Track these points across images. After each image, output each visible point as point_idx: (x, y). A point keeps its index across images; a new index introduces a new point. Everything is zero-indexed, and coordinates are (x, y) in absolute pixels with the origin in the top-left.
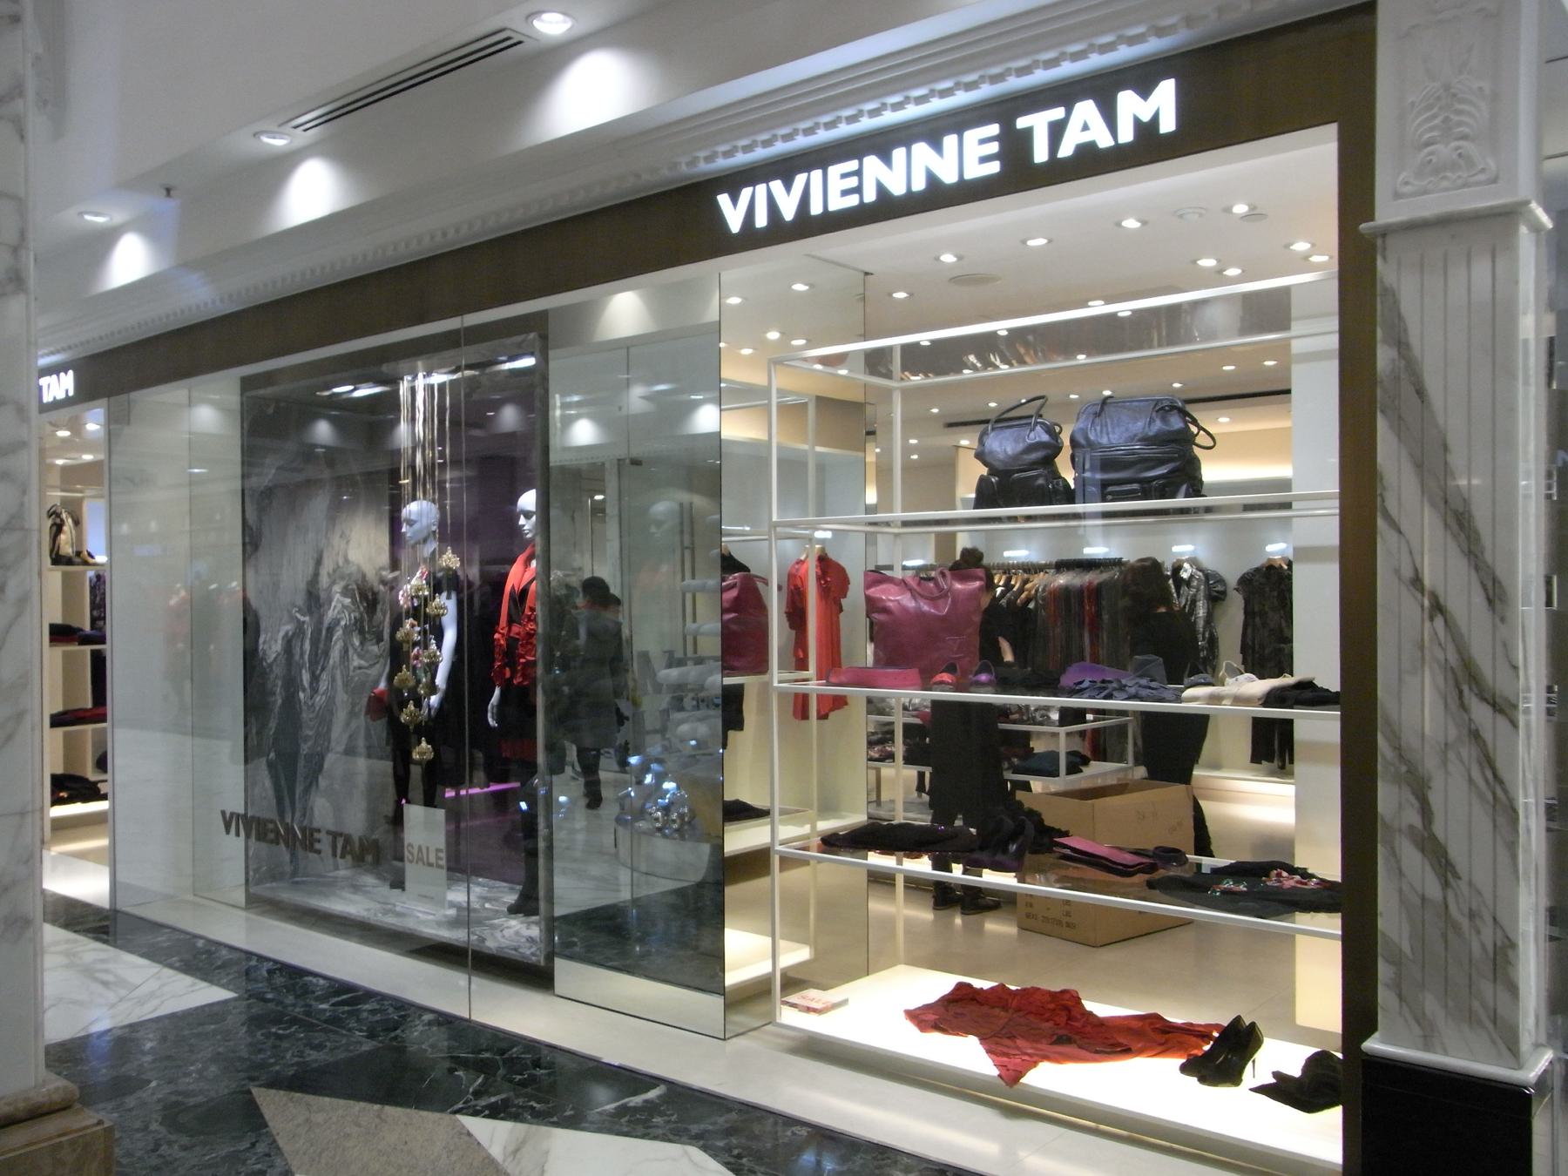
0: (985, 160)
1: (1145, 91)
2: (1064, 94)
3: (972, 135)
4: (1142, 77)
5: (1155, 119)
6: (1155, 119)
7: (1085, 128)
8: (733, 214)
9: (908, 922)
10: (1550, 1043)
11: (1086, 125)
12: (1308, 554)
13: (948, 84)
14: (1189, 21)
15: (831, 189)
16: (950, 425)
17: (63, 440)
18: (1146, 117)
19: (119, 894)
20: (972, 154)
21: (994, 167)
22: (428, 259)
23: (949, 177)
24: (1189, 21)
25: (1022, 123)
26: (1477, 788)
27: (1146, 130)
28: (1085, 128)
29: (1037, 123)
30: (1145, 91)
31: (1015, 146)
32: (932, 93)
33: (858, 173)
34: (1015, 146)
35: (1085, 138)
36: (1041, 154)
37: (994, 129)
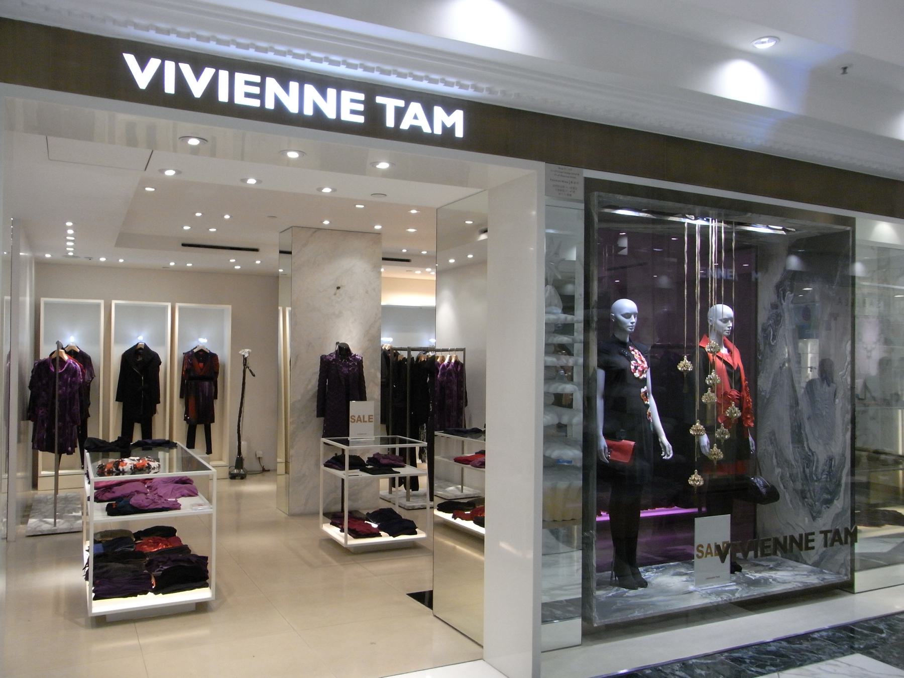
0: (353, 112)
1: (449, 111)
2: (409, 95)
3: (346, 95)
4: (450, 104)
5: (453, 126)
6: (453, 126)
7: (416, 117)
8: (457, 120)
9: (93, 461)
10: (693, 437)
11: (415, 116)
12: (578, 322)
13: (453, 80)
14: (490, 90)
15: (241, 89)
16: (184, 245)
17: (193, 147)
18: (449, 125)
19: (127, 485)
20: (349, 107)
21: (360, 119)
22: (897, 181)
23: (330, 113)
24: (490, 90)
25: (379, 100)
26: (81, 402)
27: (449, 132)
28: (416, 117)
29: (390, 104)
30: (449, 111)
31: (374, 113)
32: (290, 53)
33: (262, 85)
34: (374, 113)
35: (416, 123)
36: (390, 122)
37: (361, 97)
